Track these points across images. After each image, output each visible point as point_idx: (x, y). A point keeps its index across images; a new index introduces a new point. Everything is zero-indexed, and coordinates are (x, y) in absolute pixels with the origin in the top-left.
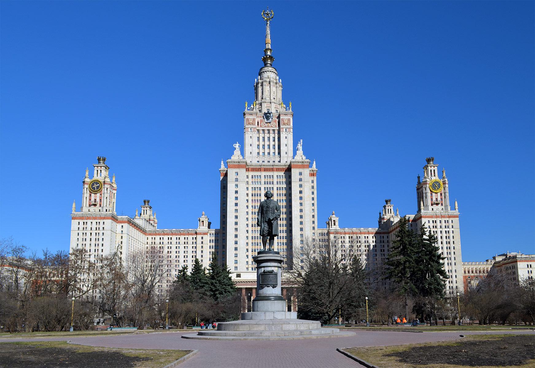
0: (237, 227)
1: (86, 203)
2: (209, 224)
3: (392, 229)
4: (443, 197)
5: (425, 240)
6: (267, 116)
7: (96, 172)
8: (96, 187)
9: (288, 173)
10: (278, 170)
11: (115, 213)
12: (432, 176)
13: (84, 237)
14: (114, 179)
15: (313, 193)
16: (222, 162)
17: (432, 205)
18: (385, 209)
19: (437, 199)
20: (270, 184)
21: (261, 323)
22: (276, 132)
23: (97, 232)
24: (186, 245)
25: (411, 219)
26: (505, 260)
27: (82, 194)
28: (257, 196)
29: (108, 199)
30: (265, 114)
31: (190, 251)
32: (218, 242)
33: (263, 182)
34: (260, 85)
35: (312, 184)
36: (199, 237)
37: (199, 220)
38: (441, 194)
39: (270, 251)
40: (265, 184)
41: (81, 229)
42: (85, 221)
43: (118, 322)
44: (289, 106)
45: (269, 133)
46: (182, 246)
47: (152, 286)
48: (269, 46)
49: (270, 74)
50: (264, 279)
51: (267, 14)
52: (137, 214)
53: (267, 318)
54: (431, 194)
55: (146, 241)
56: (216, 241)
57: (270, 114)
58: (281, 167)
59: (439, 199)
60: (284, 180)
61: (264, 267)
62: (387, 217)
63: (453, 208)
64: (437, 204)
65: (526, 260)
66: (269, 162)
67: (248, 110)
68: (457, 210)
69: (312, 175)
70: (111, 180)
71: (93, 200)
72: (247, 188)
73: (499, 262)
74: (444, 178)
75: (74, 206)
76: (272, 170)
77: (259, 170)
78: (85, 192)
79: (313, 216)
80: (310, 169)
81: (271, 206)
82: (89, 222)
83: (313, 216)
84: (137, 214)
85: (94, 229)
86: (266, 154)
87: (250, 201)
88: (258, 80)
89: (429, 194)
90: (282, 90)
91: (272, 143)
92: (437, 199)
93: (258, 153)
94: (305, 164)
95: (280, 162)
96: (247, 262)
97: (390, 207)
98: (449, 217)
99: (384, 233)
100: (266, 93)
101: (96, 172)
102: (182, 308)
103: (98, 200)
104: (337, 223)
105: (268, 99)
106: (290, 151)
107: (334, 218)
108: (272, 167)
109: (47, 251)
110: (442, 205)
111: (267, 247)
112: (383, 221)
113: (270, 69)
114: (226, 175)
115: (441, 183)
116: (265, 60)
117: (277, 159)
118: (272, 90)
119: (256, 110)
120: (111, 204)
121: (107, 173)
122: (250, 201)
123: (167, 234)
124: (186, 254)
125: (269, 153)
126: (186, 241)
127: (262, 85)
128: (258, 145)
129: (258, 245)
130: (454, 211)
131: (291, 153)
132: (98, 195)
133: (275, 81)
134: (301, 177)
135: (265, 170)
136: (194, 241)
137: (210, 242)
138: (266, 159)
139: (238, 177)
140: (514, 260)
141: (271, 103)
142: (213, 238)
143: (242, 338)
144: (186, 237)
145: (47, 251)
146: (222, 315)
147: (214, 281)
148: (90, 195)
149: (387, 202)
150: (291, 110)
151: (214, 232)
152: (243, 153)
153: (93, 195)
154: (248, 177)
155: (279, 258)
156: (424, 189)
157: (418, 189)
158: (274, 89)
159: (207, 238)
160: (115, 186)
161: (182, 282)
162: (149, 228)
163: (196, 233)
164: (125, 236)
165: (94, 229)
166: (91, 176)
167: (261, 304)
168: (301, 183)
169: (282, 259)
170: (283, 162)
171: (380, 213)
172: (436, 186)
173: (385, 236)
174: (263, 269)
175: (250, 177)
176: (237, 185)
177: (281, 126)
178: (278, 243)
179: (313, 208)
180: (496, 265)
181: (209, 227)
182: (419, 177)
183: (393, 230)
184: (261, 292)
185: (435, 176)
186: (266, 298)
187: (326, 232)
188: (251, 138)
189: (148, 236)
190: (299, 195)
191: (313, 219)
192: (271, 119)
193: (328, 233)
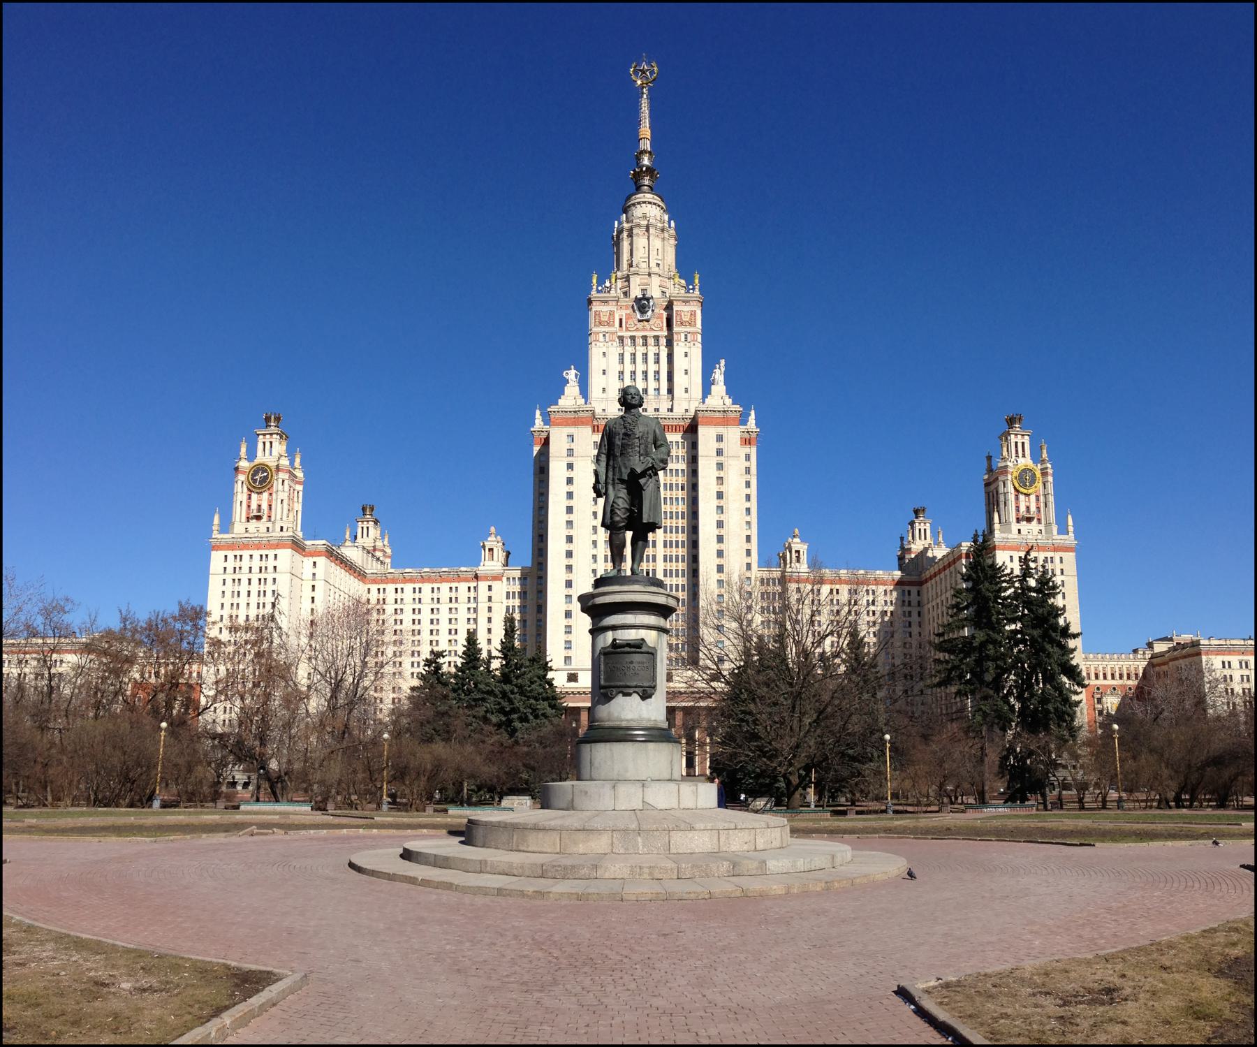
1: (239, 513)
3: (928, 574)
4: (1042, 505)
5: (1031, 589)
6: (642, 304)
7: (260, 446)
8: (261, 480)
9: (689, 435)
11: (300, 534)
12: (1018, 455)
14: (298, 460)
15: (748, 484)
16: (538, 412)
17: (1018, 521)
18: (913, 528)
19: (1028, 508)
21: (597, 823)
22: (663, 341)
23: (262, 576)
24: (453, 605)
26: (1174, 649)
27: (231, 495)
29: (286, 504)
30: (637, 300)
31: (448, 615)
34: (625, 234)
35: (747, 464)
36: (483, 586)
37: (484, 547)
38: (1038, 498)
39: (635, 577)
41: (230, 570)
42: (238, 553)
43: (275, 787)
44: (692, 283)
45: (645, 344)
46: (444, 608)
48: (646, 145)
50: (617, 669)
51: (643, 72)
52: (347, 536)
53: (622, 805)
54: (1017, 498)
57: (648, 300)
58: (675, 423)
59: (1033, 509)
61: (614, 628)
62: (917, 547)
63: (1063, 530)
64: (1029, 520)
65: (1220, 650)
67: (598, 291)
69: (747, 442)
70: (292, 462)
71: (254, 506)
73: (1161, 655)
74: (1043, 462)
75: (216, 520)
79: (748, 539)
80: (743, 428)
81: (639, 430)
82: (246, 554)
83: (748, 539)
84: (347, 536)
88: (620, 223)
89: (1012, 497)
90: (677, 247)
91: (652, 368)
92: (1028, 508)
95: (671, 410)
98: (1055, 550)
99: (911, 583)
100: (640, 253)
101: (359, 530)
102: (425, 755)
103: (265, 507)
104: (804, 557)
105: (644, 265)
107: (797, 544)
109: (128, 611)
110: (1039, 521)
111: (627, 566)
113: (649, 197)
114: (546, 442)
115: (1038, 474)
116: (637, 177)
117: (664, 405)
118: (651, 244)
119: (616, 292)
123: (411, 581)
124: (453, 627)
126: (399, 596)
127: (630, 235)
128: (621, 373)
130: (1065, 537)
131: (697, 391)
132: (265, 495)
133: (660, 225)
134: (722, 445)
136: (472, 594)
137: (508, 597)
139: (573, 446)
140: (1192, 651)
141: (649, 275)
143: (530, 886)
144: (454, 585)
145: (128, 611)
146: (525, 776)
147: (507, 688)
149: (916, 512)
150: (697, 292)
151: (518, 574)
153: (254, 496)
155: (661, 600)
156: (1001, 484)
157: (987, 485)
158: (657, 243)
159: (501, 588)
160: (300, 474)
161: (432, 687)
162: (371, 567)
163: (476, 577)
164: (320, 585)
166: (252, 455)
167: (602, 755)
168: (720, 459)
169: (672, 603)
170: (679, 411)
171: (902, 539)
172: (1026, 478)
173: (914, 590)
174: (609, 636)
176: (570, 466)
177: (676, 329)
179: (748, 519)
180: (1155, 662)
182: (989, 458)
183: (931, 578)
184: (604, 711)
186: (620, 734)
187: (776, 574)
189: (369, 586)
190: (715, 502)
191: (747, 546)
192: (650, 313)
193: (783, 581)
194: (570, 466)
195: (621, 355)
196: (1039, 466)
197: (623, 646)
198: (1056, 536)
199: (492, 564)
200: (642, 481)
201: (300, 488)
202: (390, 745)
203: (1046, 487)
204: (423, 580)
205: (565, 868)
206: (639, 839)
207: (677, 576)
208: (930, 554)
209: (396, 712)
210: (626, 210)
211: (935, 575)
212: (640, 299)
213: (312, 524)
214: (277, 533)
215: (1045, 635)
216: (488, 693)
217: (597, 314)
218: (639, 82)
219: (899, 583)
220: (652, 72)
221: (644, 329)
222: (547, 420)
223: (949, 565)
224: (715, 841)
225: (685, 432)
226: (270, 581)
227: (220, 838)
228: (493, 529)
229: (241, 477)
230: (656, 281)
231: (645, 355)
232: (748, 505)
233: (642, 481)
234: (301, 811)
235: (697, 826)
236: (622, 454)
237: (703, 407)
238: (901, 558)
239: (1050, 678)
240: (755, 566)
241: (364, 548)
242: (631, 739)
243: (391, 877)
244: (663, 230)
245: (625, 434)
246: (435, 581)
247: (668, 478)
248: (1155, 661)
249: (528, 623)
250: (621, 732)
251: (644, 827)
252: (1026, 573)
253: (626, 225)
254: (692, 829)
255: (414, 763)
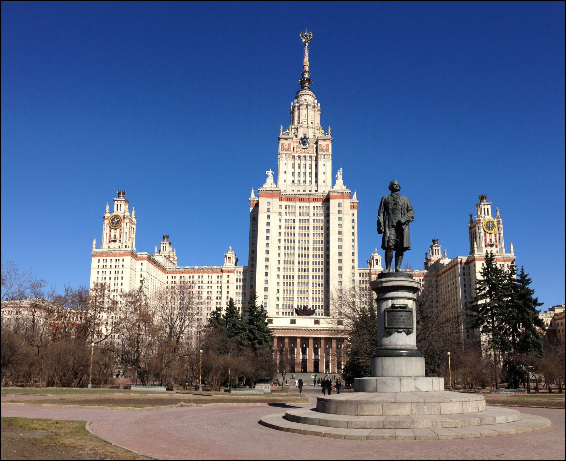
0: (268, 256)
2: (237, 260)
3: (441, 272)
4: (498, 239)
6: (304, 141)
7: (115, 206)
8: (116, 222)
9: (326, 203)
10: (315, 200)
11: (135, 249)
12: (485, 214)
13: (104, 276)
15: (353, 227)
16: (253, 191)
17: (486, 246)
18: (432, 249)
19: (491, 240)
20: (306, 215)
22: (314, 158)
23: (117, 270)
24: (210, 285)
25: (464, 261)
28: (291, 229)
29: (128, 234)
30: (302, 139)
32: (245, 282)
33: (297, 214)
34: (296, 108)
37: (226, 256)
38: (495, 235)
40: (300, 215)
41: (101, 267)
42: (105, 258)
43: (143, 378)
44: (327, 131)
45: (305, 160)
47: (181, 332)
49: (308, 97)
51: (306, 36)
52: (156, 250)
53: (405, 389)
54: (485, 235)
55: (166, 280)
56: (244, 280)
57: (307, 139)
59: (493, 240)
60: (322, 211)
61: (392, 298)
62: (434, 258)
63: (508, 251)
64: (491, 246)
66: (304, 191)
67: (283, 134)
68: (512, 253)
69: (353, 207)
70: (131, 214)
71: (112, 236)
72: (280, 220)
74: (498, 218)
75: (94, 242)
76: (308, 200)
77: (294, 199)
78: (106, 227)
82: (109, 259)
83: (353, 254)
84: (156, 250)
85: (113, 266)
86: (302, 182)
87: (283, 234)
89: (482, 235)
91: (308, 171)
92: (491, 240)
93: (293, 181)
94: (346, 194)
95: (317, 191)
96: (278, 305)
97: (437, 247)
98: (505, 261)
100: (303, 118)
101: (162, 248)
102: (220, 360)
103: (118, 236)
104: (380, 263)
105: (305, 123)
106: (327, 179)
108: (308, 197)
110: (496, 246)
112: (429, 263)
113: (308, 92)
114: (257, 205)
115: (496, 223)
116: (302, 83)
117: (314, 188)
118: (308, 113)
119: (292, 135)
120: (131, 240)
121: (127, 207)
122: (283, 234)
125: (305, 182)
126: (210, 280)
127: (299, 109)
128: (293, 173)
129: (290, 285)
130: (510, 254)
132: (118, 230)
133: (313, 105)
134: (341, 209)
135: (301, 200)
136: (220, 279)
137: (237, 281)
138: (302, 188)
139: (270, 207)
141: (308, 127)
142: (241, 277)
144: (210, 275)
147: (252, 327)
148: (110, 231)
150: (330, 136)
151: (242, 270)
152: (276, 181)
153: (113, 230)
154: (281, 207)
156: (477, 228)
157: (470, 228)
158: (311, 113)
159: (234, 277)
160: (134, 220)
162: (168, 266)
163: (222, 271)
165: (113, 266)
166: (111, 211)
167: (388, 363)
168: (340, 215)
170: (320, 191)
171: (426, 254)
172: (489, 226)
174: (390, 303)
175: (283, 207)
176: (268, 217)
177: (319, 153)
178: (313, 283)
179: (353, 244)
181: (236, 265)
182: (471, 216)
183: (442, 274)
185: (488, 215)
188: (285, 165)
190: (338, 236)
191: (353, 257)
192: (307, 145)
194: (268, 217)
195: (294, 165)
196: (496, 220)
197: (397, 307)
198: (505, 254)
199: (229, 265)
200: (403, 227)
201: (134, 227)
202: (203, 356)
203: (499, 230)
204: (194, 272)
205: (396, 423)
206: (425, 407)
207: (319, 271)
208: (441, 262)
209: (200, 341)
210: (297, 98)
211: (445, 272)
212: (303, 139)
213: (140, 245)
214: (124, 249)
215: (525, 304)
216: (242, 329)
217: (282, 145)
218: (304, 40)
219: (425, 276)
220: (310, 36)
221: (305, 153)
222: (257, 194)
223: (452, 267)
224: (461, 407)
225: (323, 202)
226: (120, 272)
227: (244, 405)
228: (230, 248)
229: (107, 221)
230: (311, 130)
231: (305, 165)
232: (353, 237)
233: (403, 227)
234: (160, 391)
235: (453, 400)
236: (393, 213)
237: (332, 190)
238: (426, 264)
239: (527, 326)
240: (356, 267)
241: (165, 256)
242: (400, 355)
243: (278, 428)
244: (314, 107)
245: (394, 204)
246: (201, 272)
247: (315, 224)
248: (556, 317)
249: (247, 294)
250: (398, 352)
251: (427, 401)
252: (513, 272)
253: (297, 105)
254: (451, 401)
255: (215, 366)
